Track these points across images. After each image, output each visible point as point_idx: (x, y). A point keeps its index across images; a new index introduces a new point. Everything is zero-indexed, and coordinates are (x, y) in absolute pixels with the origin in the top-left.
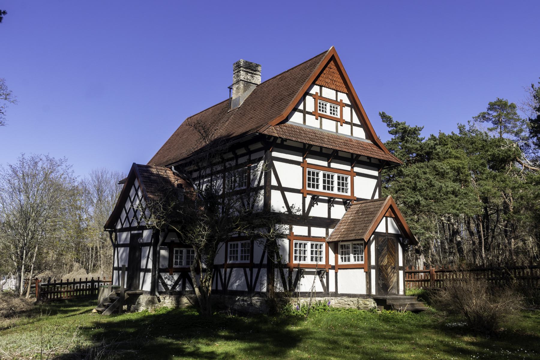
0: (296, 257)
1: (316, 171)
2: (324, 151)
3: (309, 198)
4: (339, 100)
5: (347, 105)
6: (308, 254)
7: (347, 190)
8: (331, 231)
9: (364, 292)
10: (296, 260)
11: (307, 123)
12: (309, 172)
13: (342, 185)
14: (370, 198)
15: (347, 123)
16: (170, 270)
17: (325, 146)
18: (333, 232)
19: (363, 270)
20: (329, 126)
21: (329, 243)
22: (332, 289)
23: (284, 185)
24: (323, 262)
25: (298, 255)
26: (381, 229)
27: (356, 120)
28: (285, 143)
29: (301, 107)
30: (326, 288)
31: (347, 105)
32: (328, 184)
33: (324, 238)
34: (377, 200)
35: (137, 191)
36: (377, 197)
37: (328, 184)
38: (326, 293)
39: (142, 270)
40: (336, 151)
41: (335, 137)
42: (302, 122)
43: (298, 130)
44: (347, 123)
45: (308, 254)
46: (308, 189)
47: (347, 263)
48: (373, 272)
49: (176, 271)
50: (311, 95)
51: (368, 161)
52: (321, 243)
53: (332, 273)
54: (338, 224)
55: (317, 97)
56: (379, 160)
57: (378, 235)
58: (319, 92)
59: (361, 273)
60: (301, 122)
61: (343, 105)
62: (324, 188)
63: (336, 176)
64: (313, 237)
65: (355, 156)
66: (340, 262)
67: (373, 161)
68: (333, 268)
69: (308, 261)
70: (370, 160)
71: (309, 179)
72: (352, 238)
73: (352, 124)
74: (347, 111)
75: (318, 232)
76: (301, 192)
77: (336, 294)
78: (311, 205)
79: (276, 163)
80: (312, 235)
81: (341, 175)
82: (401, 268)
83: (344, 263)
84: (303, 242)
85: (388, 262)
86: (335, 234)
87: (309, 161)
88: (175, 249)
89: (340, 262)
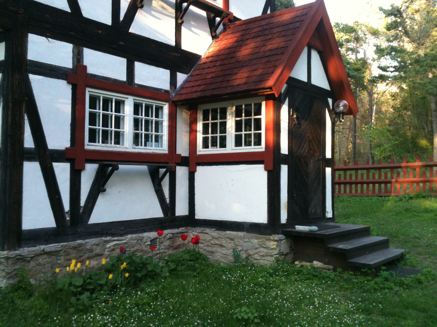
0: (93, 133)
3: (90, 172)
6: (128, 128)
8: (181, 78)
9: (261, 216)
10: (92, 139)
18: (186, 82)
19: (262, 166)
21: (175, 106)
22: (181, 209)
24: (163, 148)
25: (100, 127)
26: (300, 73)
30: (168, 207)
33: (166, 91)
38: (170, 219)
45: (128, 128)
46: (89, 146)
47: (218, 150)
48: (284, 169)
52: (159, 103)
53: (182, 172)
57: (294, 83)
59: (258, 174)
68: (183, 161)
69: (127, 145)
75: (151, 76)
77: (190, 220)
78: (99, 187)
80: (138, 80)
82: (330, 163)
84: (115, 96)
85: (310, 149)
86: (192, 84)
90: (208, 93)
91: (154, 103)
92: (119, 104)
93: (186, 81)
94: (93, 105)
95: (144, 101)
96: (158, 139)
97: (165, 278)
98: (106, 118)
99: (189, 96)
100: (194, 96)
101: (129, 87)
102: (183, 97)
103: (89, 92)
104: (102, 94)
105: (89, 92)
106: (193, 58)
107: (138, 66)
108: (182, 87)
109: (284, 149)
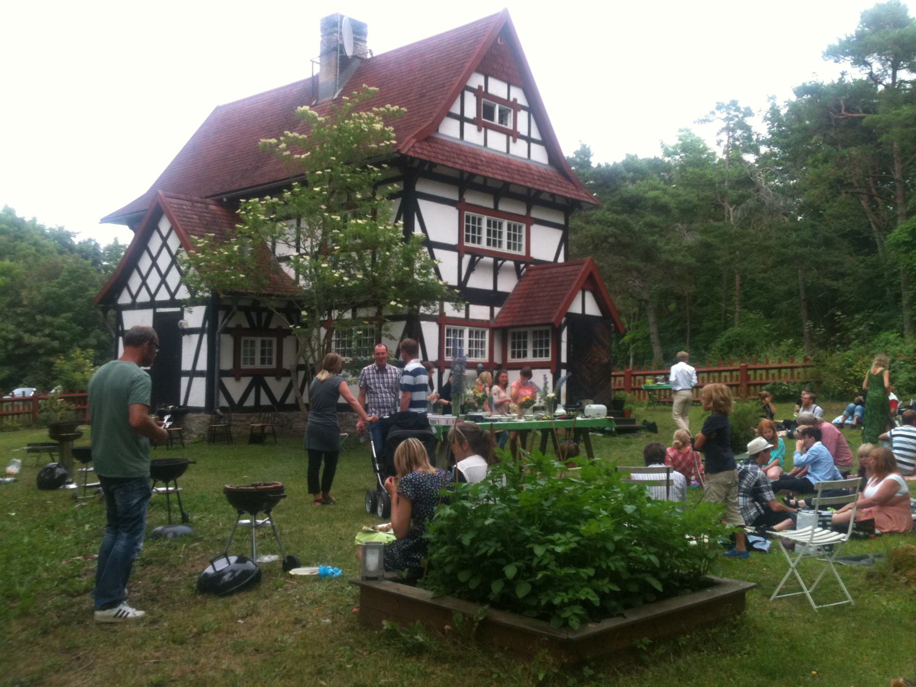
1: (477, 215)
2: (489, 184)
3: (467, 258)
4: (511, 99)
5: (524, 108)
7: (520, 246)
8: (497, 310)
11: (467, 137)
12: (468, 217)
13: (513, 238)
14: (551, 259)
15: (522, 137)
16: (236, 373)
17: (491, 175)
20: (497, 142)
23: (433, 238)
27: (535, 134)
28: (435, 170)
29: (456, 109)
31: (524, 108)
32: (494, 235)
34: (561, 265)
35: (165, 239)
36: (561, 259)
37: (494, 235)
39: (201, 374)
40: (506, 185)
41: (505, 163)
42: (458, 136)
43: (459, 150)
44: (522, 137)
46: (466, 244)
49: (246, 373)
50: (471, 90)
51: (551, 200)
52: (483, 329)
54: (507, 301)
55: (481, 94)
56: (567, 199)
57: (572, 317)
58: (483, 84)
59: (535, 230)
60: (457, 135)
61: (516, 107)
62: (489, 244)
63: (505, 224)
64: (473, 320)
65: (533, 193)
66: (510, 360)
67: (558, 201)
70: (554, 199)
71: (468, 227)
72: (538, 322)
73: (529, 140)
74: (523, 116)
75: (480, 312)
76: (459, 249)
78: (471, 269)
79: (423, 204)
80: (471, 317)
81: (513, 223)
83: (516, 360)
84: (458, 328)
87: (470, 199)
88: (243, 339)
89: (510, 360)
90: (515, 324)
91: (480, 330)
92: (461, 332)
93: (500, 313)
94: (468, 221)
95: (475, 329)
96: (483, 353)
97: (488, 498)
98: (474, 228)
99: (503, 325)
100: (507, 324)
101: (467, 321)
102: (498, 325)
103: (466, 213)
104: (453, 327)
105: (446, 327)
106: (505, 295)
107: (472, 307)
108: (497, 317)
109: (564, 359)
